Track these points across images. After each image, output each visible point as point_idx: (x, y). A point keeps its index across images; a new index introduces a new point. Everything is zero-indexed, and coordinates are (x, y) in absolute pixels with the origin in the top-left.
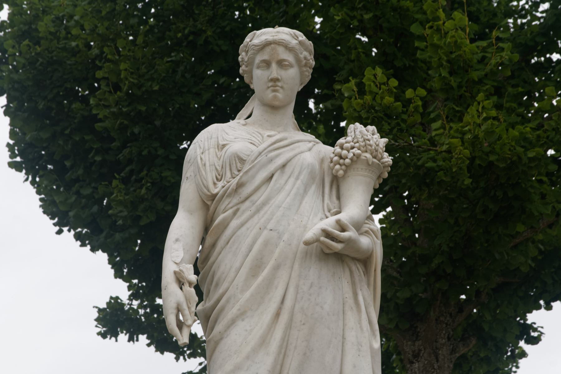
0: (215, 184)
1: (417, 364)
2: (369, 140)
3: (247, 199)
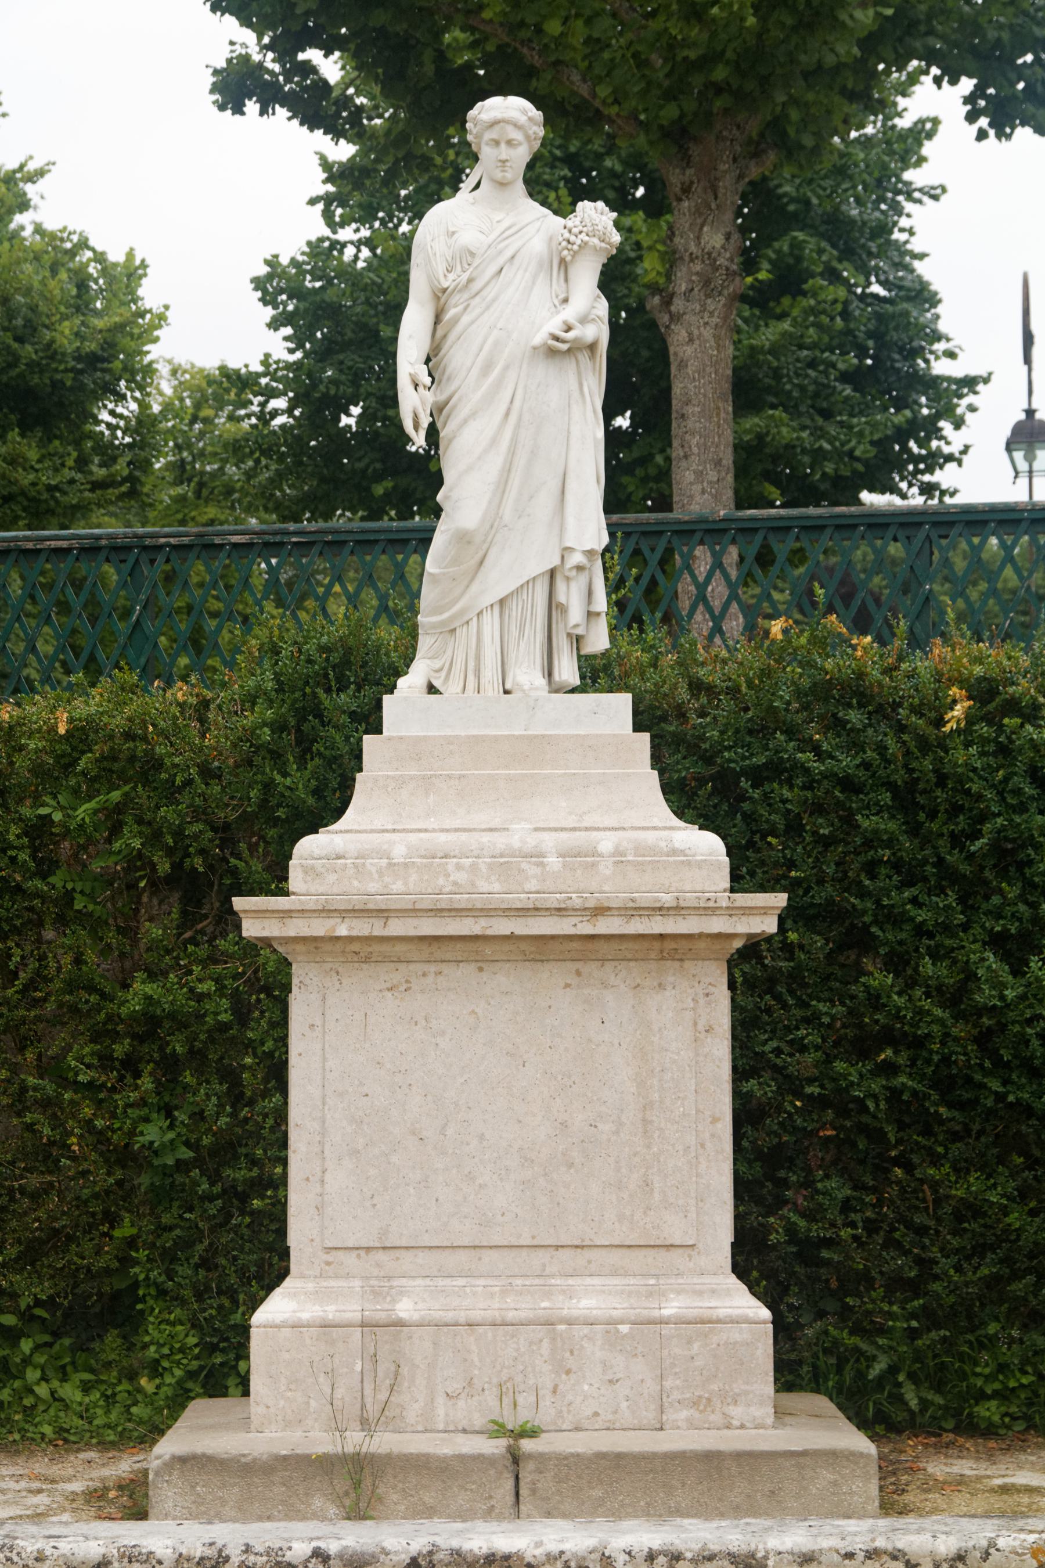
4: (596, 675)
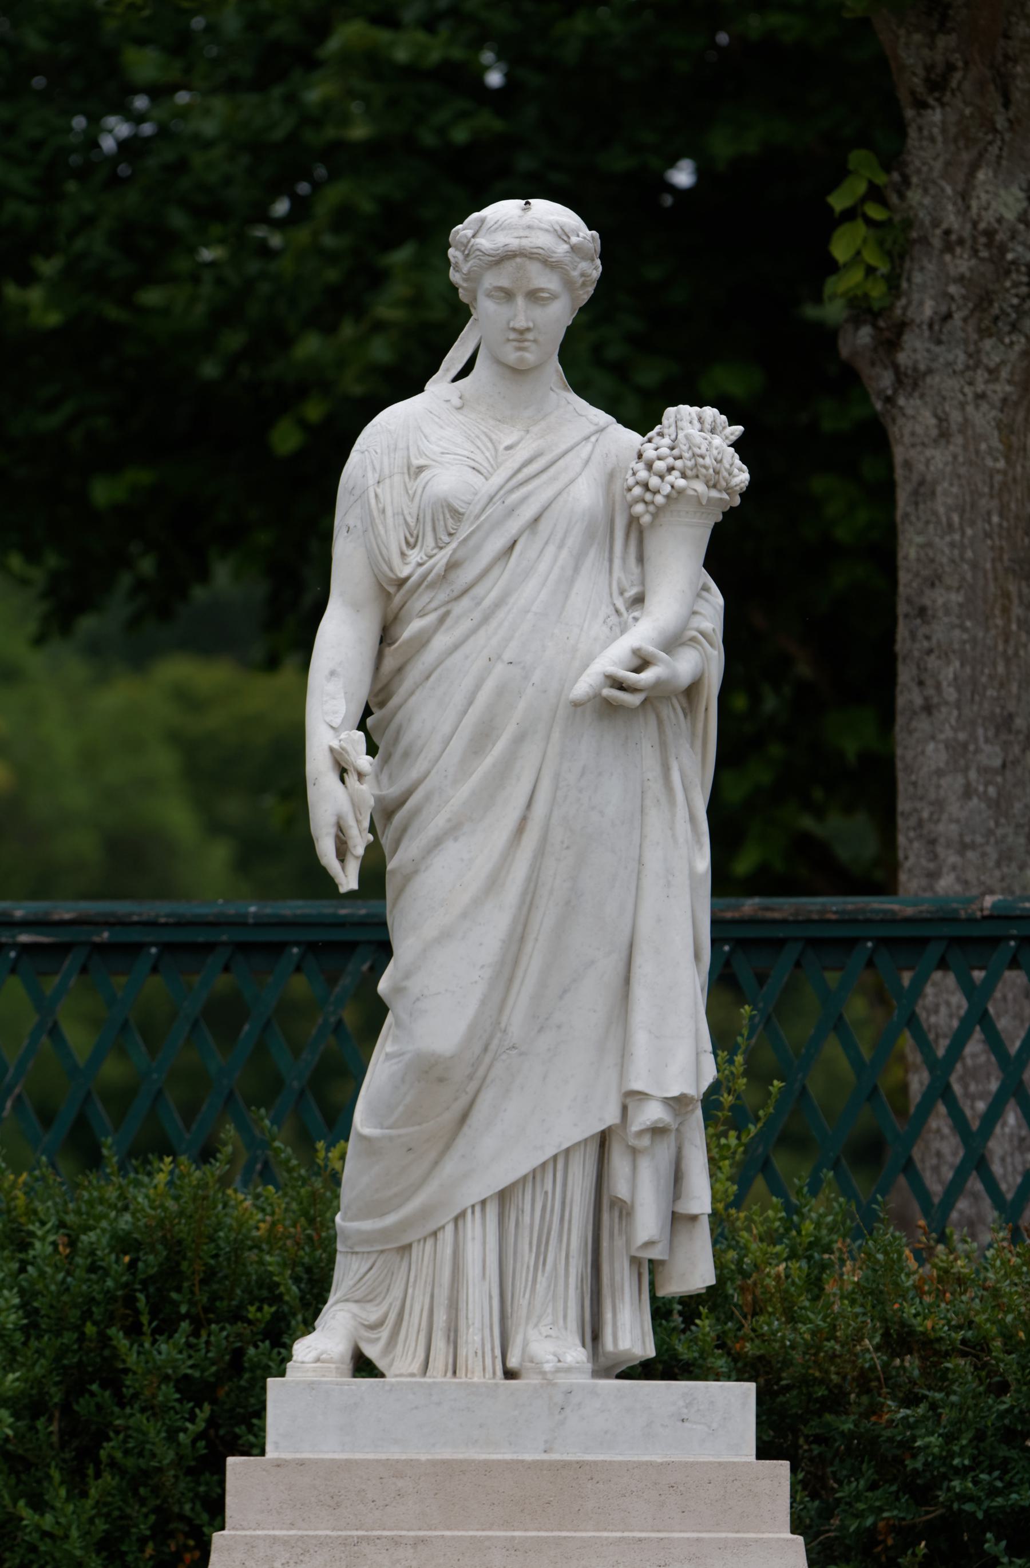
0: (403, 554)
1: (938, 111)
2: (703, 457)
3: (465, 592)
4: (685, 1343)
